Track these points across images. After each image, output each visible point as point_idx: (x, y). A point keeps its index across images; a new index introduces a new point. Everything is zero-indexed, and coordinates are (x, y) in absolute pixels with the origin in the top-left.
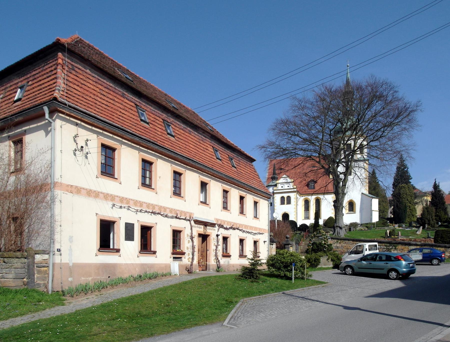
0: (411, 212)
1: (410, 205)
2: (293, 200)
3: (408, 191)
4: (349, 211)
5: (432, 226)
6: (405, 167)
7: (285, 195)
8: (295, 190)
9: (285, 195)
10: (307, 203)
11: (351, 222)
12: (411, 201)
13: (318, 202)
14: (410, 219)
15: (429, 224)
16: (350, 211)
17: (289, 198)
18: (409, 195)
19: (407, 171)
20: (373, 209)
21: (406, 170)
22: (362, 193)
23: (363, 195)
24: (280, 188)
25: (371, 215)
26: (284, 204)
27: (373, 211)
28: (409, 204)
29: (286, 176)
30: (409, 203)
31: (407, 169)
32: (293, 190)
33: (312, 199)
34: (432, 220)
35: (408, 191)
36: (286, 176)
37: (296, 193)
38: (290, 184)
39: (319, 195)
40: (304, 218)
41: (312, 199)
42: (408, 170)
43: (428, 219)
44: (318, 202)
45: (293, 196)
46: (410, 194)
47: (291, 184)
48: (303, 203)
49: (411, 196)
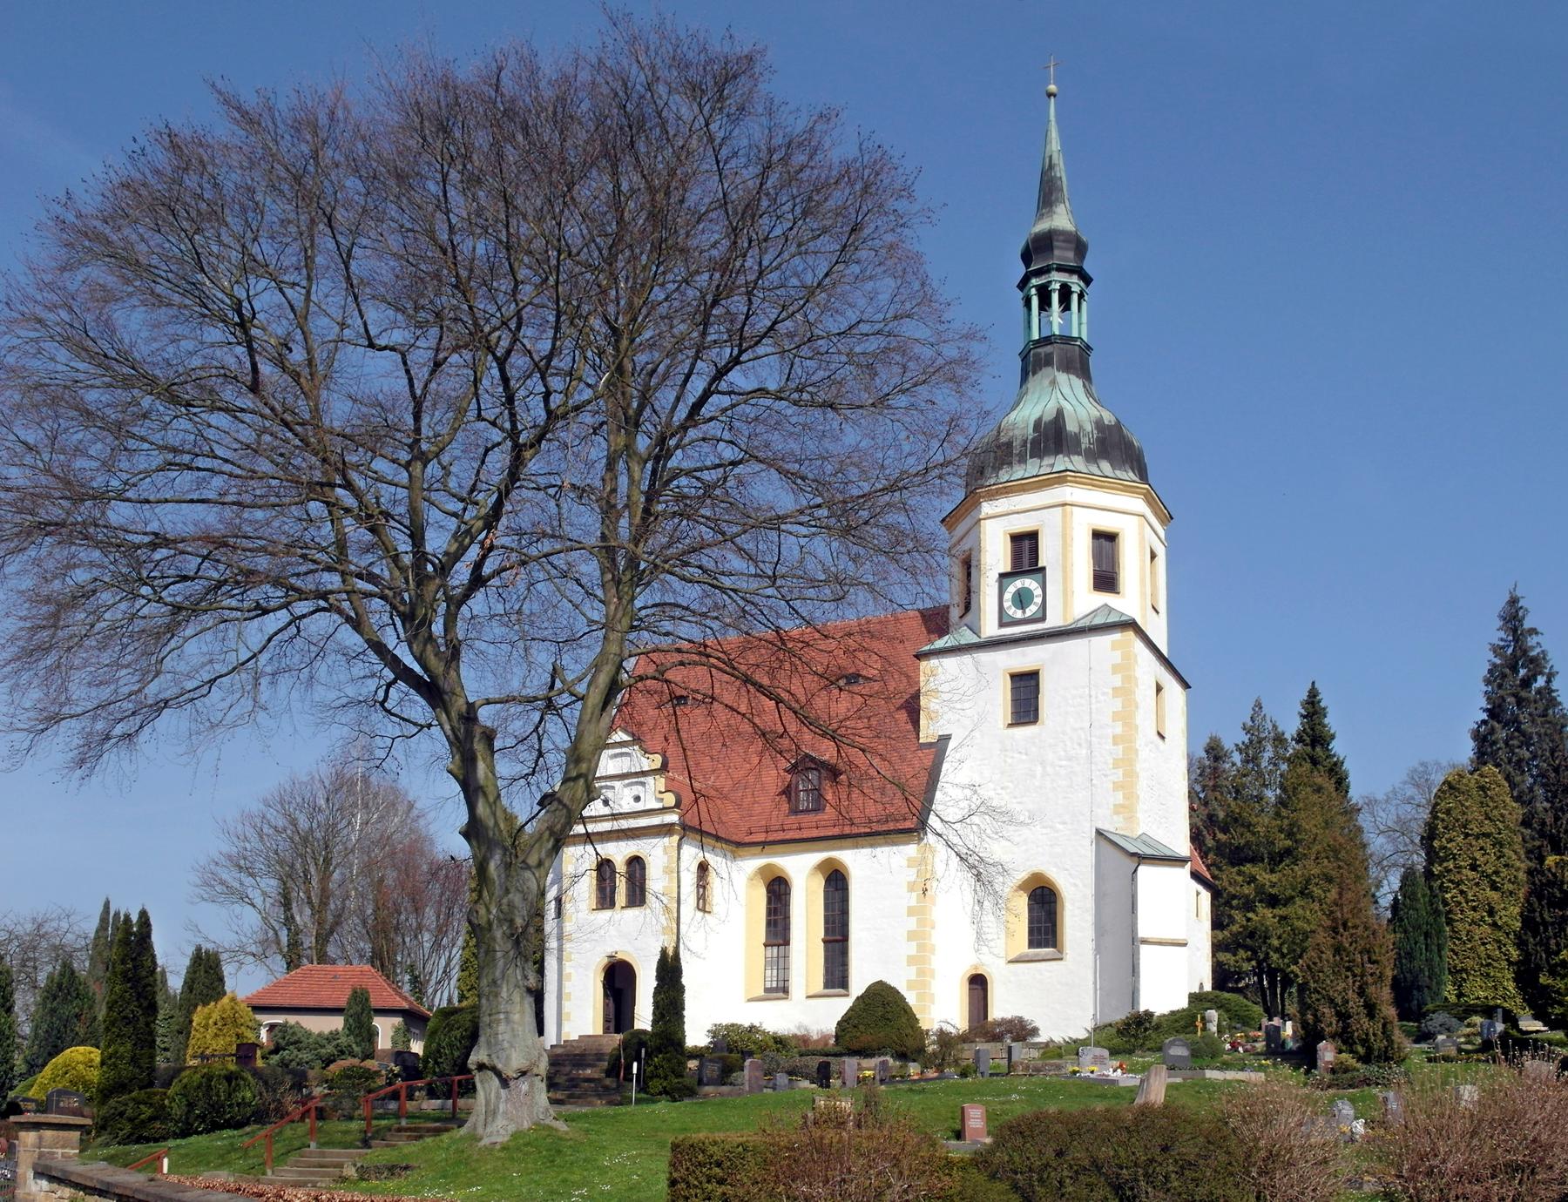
0: (1499, 941)
1: (1495, 896)
2: (656, 881)
3: (1475, 814)
4: (1032, 944)
5: (1369, 1050)
6: (1536, 664)
7: (618, 852)
8: (673, 818)
9: (618, 852)
10: (778, 890)
11: (1027, 1017)
12: (1496, 873)
13: (836, 882)
14: (1495, 988)
15: (1345, 1038)
16: (1039, 945)
17: (636, 863)
18: (1487, 835)
19: (1547, 692)
20: (1142, 933)
21: (1541, 682)
22: (1099, 833)
23: (1105, 845)
24: (627, 805)
25: (1135, 970)
26: (612, 905)
27: (1145, 942)
28: (1489, 893)
29: (626, 738)
30: (1485, 884)
31: (1549, 681)
32: (655, 820)
33: (801, 868)
34: (1363, 1011)
35: (1475, 814)
36: (626, 738)
37: (676, 838)
38: (643, 784)
39: (841, 848)
40: (761, 992)
41: (801, 868)
42: (1554, 685)
43: (1339, 1000)
44: (836, 882)
45: (656, 853)
46: (1488, 827)
47: (650, 780)
48: (819, 883)
49: (1499, 844)
